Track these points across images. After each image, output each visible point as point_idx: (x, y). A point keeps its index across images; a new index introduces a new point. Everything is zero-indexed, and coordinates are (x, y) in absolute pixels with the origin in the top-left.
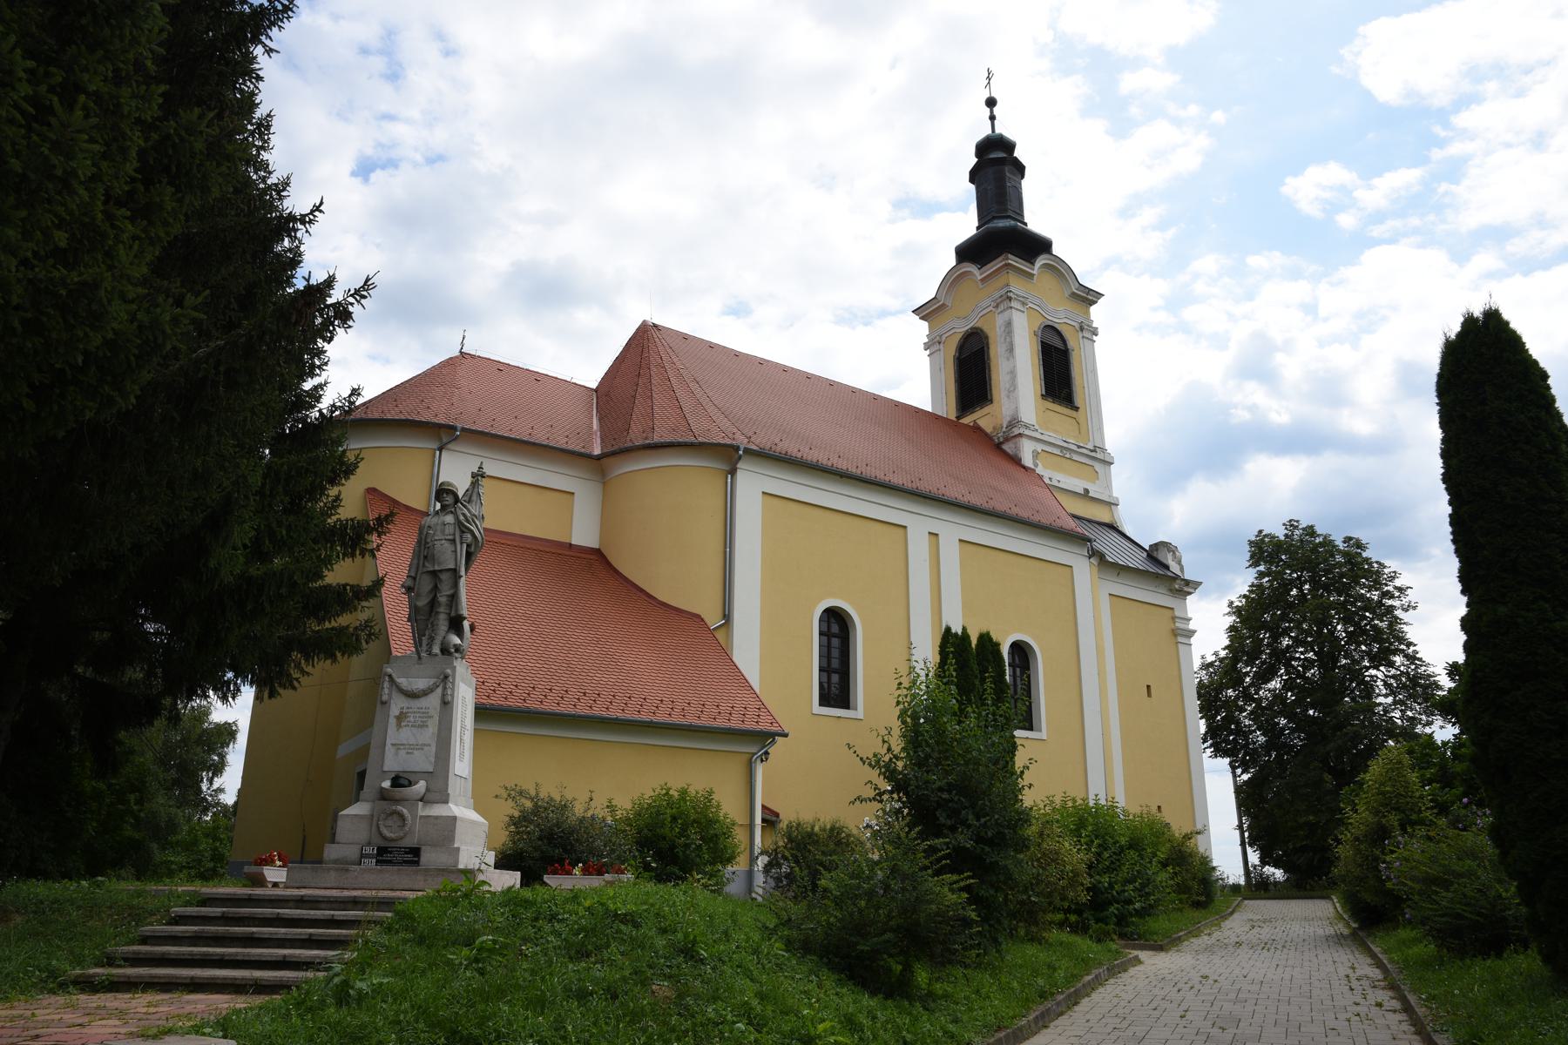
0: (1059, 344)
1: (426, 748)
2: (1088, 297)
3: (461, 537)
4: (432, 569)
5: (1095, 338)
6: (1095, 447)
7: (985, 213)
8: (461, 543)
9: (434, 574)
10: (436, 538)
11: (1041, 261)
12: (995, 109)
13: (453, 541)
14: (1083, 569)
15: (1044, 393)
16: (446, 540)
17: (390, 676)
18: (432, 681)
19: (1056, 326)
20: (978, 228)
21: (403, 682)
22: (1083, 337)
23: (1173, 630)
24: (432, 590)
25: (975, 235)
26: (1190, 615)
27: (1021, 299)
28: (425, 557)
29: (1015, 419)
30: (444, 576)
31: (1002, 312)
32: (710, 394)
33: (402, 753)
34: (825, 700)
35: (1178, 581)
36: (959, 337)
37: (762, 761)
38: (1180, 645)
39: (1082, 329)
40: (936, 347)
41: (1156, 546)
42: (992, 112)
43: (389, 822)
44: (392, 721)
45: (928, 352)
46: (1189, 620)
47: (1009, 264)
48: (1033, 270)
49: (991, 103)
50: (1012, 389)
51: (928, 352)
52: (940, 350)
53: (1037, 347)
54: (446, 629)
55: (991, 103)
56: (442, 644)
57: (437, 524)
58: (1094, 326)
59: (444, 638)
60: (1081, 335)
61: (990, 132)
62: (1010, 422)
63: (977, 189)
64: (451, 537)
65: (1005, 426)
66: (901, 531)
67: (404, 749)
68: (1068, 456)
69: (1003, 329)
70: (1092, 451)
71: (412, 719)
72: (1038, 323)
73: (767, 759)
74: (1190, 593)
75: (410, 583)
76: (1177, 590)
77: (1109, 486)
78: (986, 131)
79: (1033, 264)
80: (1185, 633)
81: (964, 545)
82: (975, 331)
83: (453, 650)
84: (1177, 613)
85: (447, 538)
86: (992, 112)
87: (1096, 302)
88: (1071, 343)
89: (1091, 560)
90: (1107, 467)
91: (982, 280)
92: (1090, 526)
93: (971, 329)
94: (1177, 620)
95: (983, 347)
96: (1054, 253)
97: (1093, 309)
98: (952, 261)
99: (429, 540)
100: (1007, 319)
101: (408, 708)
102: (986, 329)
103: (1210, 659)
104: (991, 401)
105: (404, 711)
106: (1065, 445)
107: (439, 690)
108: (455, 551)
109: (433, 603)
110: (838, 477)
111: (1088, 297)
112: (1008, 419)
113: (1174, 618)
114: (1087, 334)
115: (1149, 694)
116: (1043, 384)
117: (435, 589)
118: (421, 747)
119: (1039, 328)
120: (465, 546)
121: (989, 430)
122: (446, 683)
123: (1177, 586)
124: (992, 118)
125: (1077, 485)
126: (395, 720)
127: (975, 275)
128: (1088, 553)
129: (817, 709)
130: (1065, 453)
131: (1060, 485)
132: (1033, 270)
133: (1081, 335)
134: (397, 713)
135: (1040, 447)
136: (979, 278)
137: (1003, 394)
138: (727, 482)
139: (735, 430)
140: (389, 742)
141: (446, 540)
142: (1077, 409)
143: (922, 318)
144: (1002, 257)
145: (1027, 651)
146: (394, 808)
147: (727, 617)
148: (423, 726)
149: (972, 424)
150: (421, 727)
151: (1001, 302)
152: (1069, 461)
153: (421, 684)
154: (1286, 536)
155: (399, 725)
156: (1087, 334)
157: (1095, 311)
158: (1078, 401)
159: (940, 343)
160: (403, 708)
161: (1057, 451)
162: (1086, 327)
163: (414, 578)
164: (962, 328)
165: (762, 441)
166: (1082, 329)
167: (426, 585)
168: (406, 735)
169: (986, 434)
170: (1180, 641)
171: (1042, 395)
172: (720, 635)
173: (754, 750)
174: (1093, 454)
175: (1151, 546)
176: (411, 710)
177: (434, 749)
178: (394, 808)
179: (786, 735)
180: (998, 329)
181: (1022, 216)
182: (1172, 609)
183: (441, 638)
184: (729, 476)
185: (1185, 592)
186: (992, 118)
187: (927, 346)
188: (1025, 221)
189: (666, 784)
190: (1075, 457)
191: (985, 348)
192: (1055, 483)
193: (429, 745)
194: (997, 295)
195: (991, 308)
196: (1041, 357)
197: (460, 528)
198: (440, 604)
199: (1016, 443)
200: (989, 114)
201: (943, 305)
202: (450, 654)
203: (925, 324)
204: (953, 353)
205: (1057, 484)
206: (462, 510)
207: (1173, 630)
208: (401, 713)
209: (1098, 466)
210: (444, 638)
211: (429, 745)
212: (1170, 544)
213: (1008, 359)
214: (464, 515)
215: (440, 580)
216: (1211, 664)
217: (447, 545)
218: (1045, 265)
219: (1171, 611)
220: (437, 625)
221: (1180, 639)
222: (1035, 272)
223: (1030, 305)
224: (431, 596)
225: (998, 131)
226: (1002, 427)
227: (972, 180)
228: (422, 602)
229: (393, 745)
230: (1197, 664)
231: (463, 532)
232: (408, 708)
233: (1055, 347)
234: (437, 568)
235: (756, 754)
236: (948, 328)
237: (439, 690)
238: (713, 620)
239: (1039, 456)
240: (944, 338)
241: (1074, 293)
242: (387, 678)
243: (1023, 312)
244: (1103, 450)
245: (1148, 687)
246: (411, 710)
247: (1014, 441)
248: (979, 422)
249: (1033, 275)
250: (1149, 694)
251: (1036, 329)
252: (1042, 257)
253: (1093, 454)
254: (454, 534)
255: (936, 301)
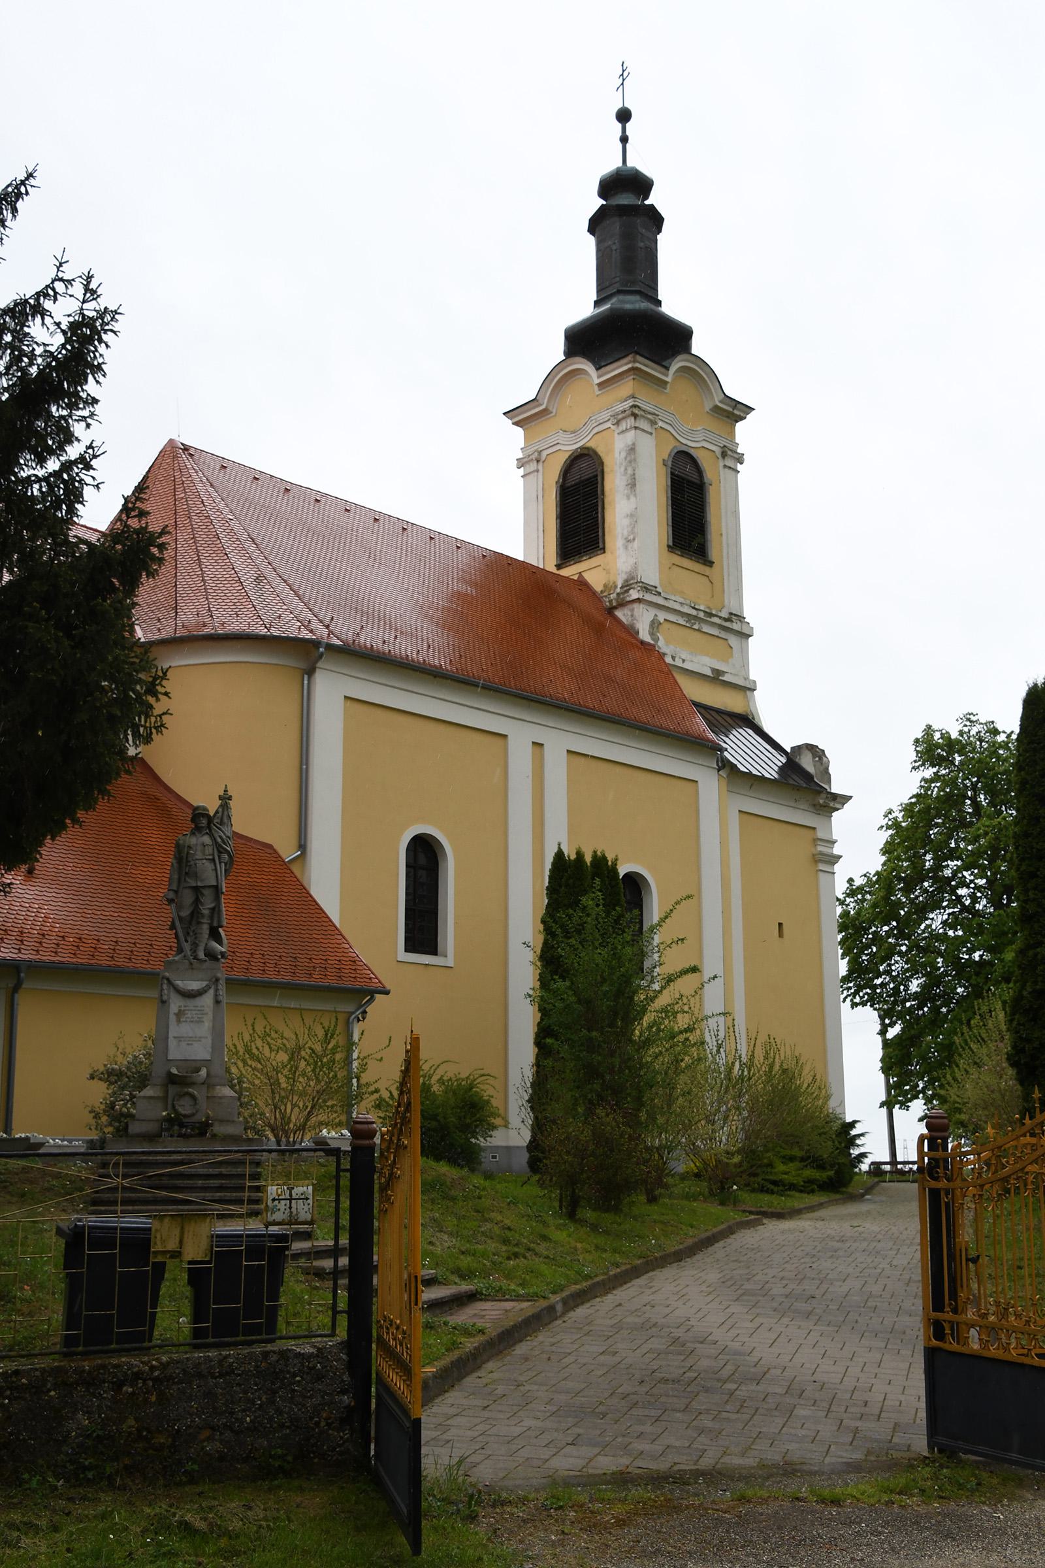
0: (694, 477)
1: (203, 1039)
2: (735, 411)
3: (219, 856)
4: (195, 885)
5: (739, 467)
6: (731, 614)
7: (607, 284)
8: (220, 863)
9: (196, 889)
10: (197, 857)
11: (677, 364)
12: (628, 125)
13: (213, 860)
14: (709, 783)
15: (671, 544)
16: (206, 859)
17: (168, 979)
18: (204, 984)
19: (692, 452)
20: (597, 303)
21: (179, 983)
22: (725, 466)
23: (814, 855)
24: (193, 902)
25: (592, 317)
26: (834, 837)
27: (650, 416)
28: (186, 873)
29: (633, 578)
30: (206, 892)
31: (623, 432)
32: (271, 558)
33: (183, 1044)
34: (411, 947)
35: (824, 795)
36: (567, 455)
37: (359, 1020)
38: (821, 874)
39: (724, 455)
40: (533, 466)
41: (797, 749)
42: (624, 130)
43: (182, 1102)
44: (172, 1018)
45: (521, 471)
46: (834, 842)
47: (637, 369)
48: (667, 376)
49: (624, 116)
50: (631, 537)
51: (521, 471)
52: (537, 471)
53: (665, 481)
54: (207, 936)
55: (624, 116)
56: (205, 950)
57: (197, 844)
58: (739, 451)
59: (206, 944)
60: (721, 464)
61: (620, 164)
62: (626, 581)
63: (599, 244)
64: (211, 857)
65: (619, 586)
66: (498, 742)
67: (184, 1041)
68: (696, 627)
69: (623, 454)
70: (726, 620)
71: (189, 1015)
72: (667, 451)
73: (364, 1018)
74: (837, 809)
75: (171, 895)
76: (821, 806)
77: (745, 665)
78: (611, 163)
79: (667, 368)
80: (827, 858)
81: (573, 757)
82: (586, 452)
83: (220, 957)
84: (820, 834)
85: (207, 857)
86: (624, 130)
87: (745, 418)
88: (709, 475)
89: (720, 772)
90: (744, 641)
91: (599, 385)
92: (719, 718)
93: (582, 448)
94: (819, 843)
95: (597, 476)
96: (693, 352)
97: (739, 426)
98: (556, 351)
99: (190, 859)
100: (630, 443)
101: (185, 1006)
102: (601, 451)
103: (859, 882)
104: (603, 550)
105: (182, 1009)
106: (694, 612)
107: (211, 992)
108: (216, 870)
109: (195, 914)
110: (431, 677)
111: (735, 411)
112: (624, 577)
113: (816, 841)
114: (729, 463)
115: (781, 935)
116: (671, 532)
117: (197, 902)
118: (199, 1039)
119: (669, 455)
120: (223, 864)
121: (598, 588)
122: (217, 986)
123: (821, 801)
124: (624, 139)
125: (703, 664)
126: (174, 1017)
127: (589, 375)
128: (718, 765)
129: (403, 955)
130: (693, 620)
131: (686, 666)
132: (667, 376)
133: (721, 464)
134: (176, 1011)
135: (662, 616)
136: (597, 381)
137: (620, 543)
138: (303, 683)
139: (310, 616)
140: (171, 1035)
141: (206, 859)
142: (710, 564)
143: (516, 424)
144: (630, 358)
145: (639, 881)
146: (186, 1090)
147: (303, 846)
148: (200, 1021)
149: (575, 578)
150: (197, 1022)
151: (623, 418)
152: (696, 633)
153: (195, 985)
154: (961, 733)
155: (179, 1021)
156: (729, 463)
157: (742, 430)
158: (713, 554)
159: (538, 461)
160: (180, 1007)
161: (681, 621)
162: (729, 453)
163: (176, 892)
164: (570, 446)
165: (345, 630)
166: (724, 455)
167: (188, 898)
168: (185, 1029)
169: (594, 593)
170: (821, 868)
171: (669, 546)
172: (296, 869)
173: (351, 1008)
174: (727, 624)
175: (792, 748)
176: (187, 1008)
177: (209, 1041)
178: (186, 1090)
179: (387, 993)
180: (617, 455)
181: (655, 289)
182: (814, 829)
183: (204, 945)
184: (306, 677)
185: (832, 808)
186: (624, 139)
187: (521, 464)
188: (660, 298)
189: (459, 1074)
190: (706, 629)
191: (599, 478)
192: (678, 663)
193: (207, 1038)
194: (620, 407)
195: (608, 425)
196: (670, 495)
197: (217, 848)
198: (203, 916)
199: (632, 610)
200: (620, 134)
201: (545, 412)
202: (217, 960)
203: (519, 432)
204: (556, 479)
205: (681, 665)
206: (218, 833)
207: (814, 855)
208: (180, 1011)
209: (733, 640)
210: (206, 944)
211: (207, 1038)
212: (817, 747)
213: (628, 498)
214: (220, 837)
215: (202, 894)
216: (860, 889)
217: (209, 866)
218: (684, 369)
219: (812, 832)
220: (201, 934)
221: (822, 867)
222: (669, 379)
223: (660, 424)
224: (192, 908)
225: (630, 164)
226: (616, 587)
227: (592, 229)
228: (185, 913)
229: (175, 1037)
230: (841, 888)
231: (221, 853)
232: (185, 1006)
233: (689, 481)
234: (199, 884)
235: (353, 1013)
236: (551, 441)
237: (211, 992)
238: (288, 852)
239: (660, 627)
240: (544, 454)
241: (716, 407)
242: (166, 982)
243: (651, 434)
244: (741, 618)
245: (780, 925)
246: (187, 1008)
247: (630, 606)
248: (587, 576)
249: (666, 383)
250: (781, 935)
251: (666, 457)
252: (679, 358)
253: (727, 624)
254: (213, 855)
255: (535, 403)
